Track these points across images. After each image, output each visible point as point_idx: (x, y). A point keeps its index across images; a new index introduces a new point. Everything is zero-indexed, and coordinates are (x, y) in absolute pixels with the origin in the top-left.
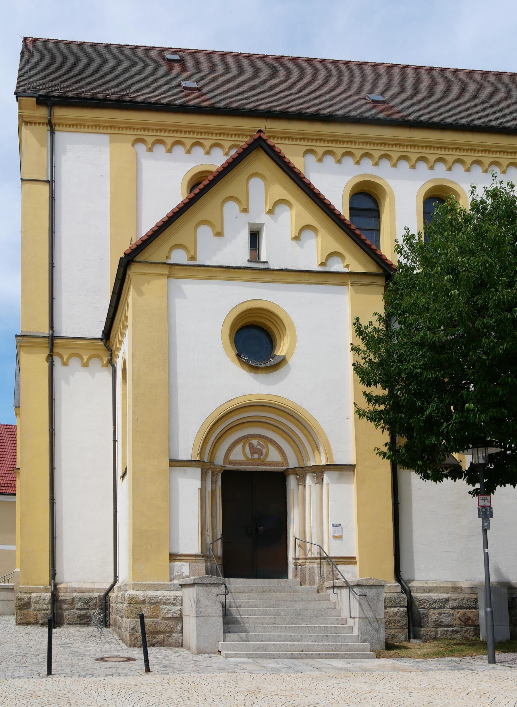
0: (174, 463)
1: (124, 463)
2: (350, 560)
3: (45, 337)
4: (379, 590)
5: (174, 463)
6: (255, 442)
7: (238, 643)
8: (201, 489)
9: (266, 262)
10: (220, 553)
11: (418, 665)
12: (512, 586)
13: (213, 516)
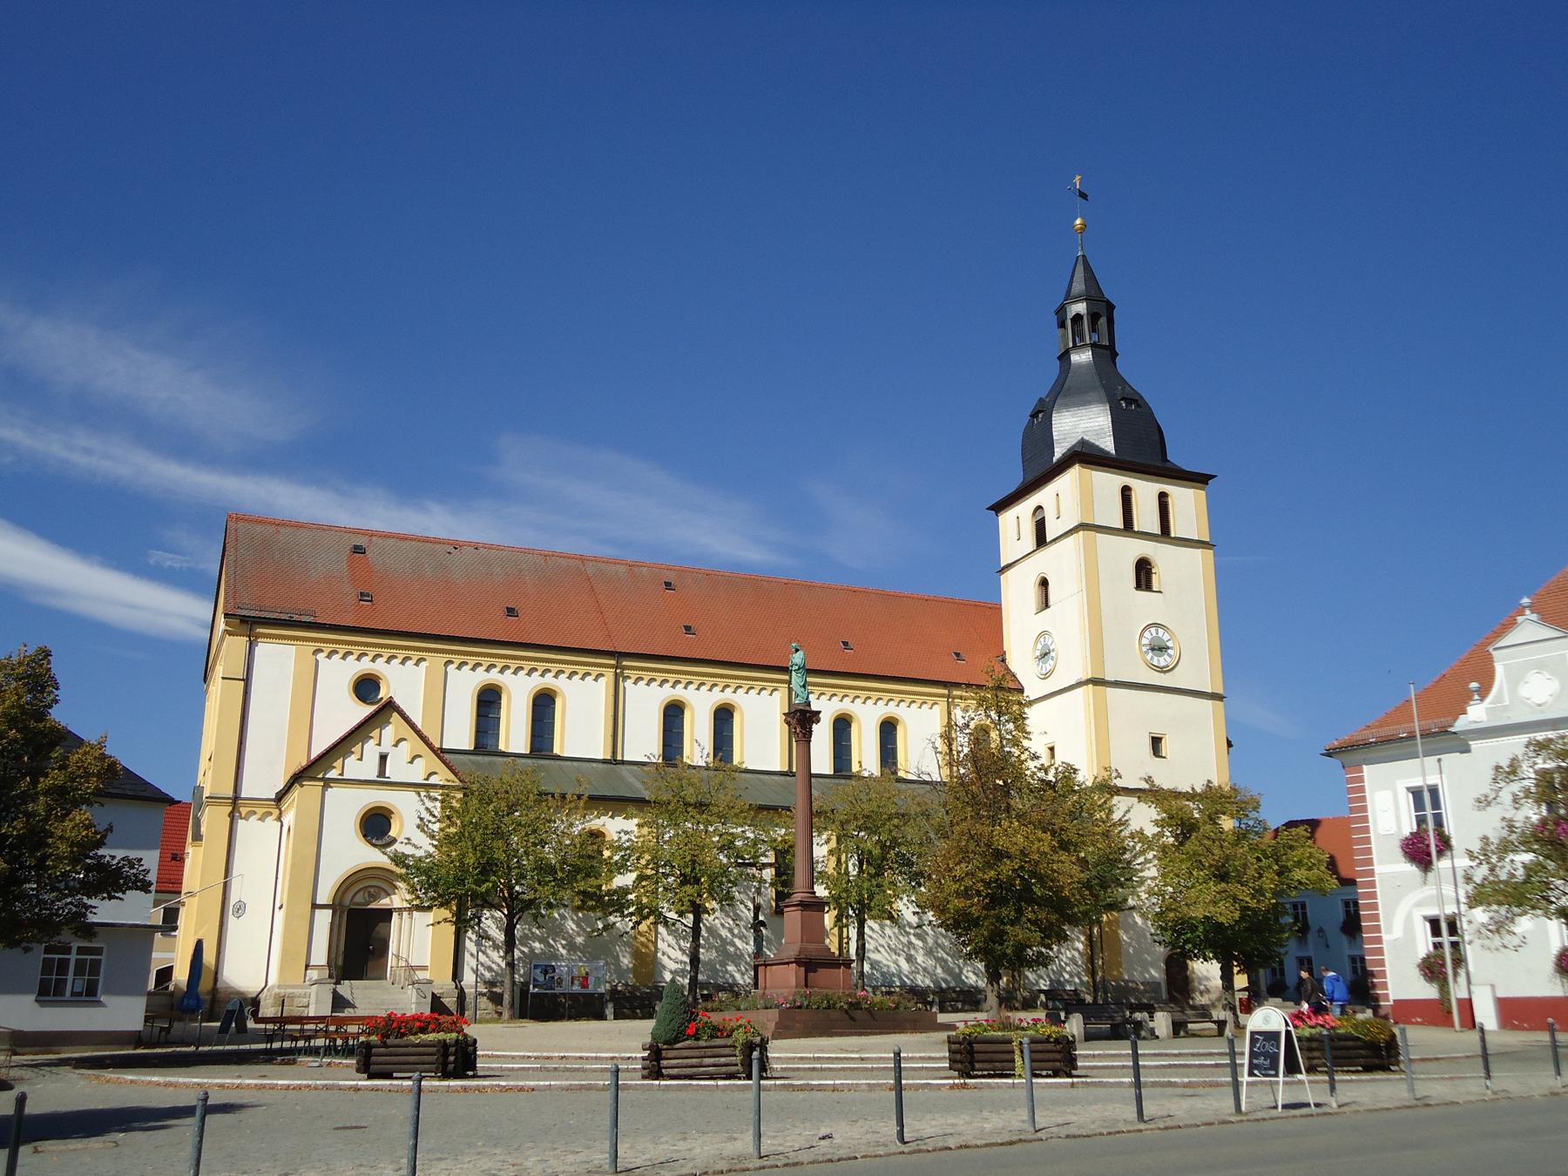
1: (282, 899)
2: (424, 968)
3: (229, 798)
6: (372, 890)
7: (508, 1053)
8: (331, 923)
9: (388, 778)
10: (774, 897)
12: (232, 988)
13: (338, 940)
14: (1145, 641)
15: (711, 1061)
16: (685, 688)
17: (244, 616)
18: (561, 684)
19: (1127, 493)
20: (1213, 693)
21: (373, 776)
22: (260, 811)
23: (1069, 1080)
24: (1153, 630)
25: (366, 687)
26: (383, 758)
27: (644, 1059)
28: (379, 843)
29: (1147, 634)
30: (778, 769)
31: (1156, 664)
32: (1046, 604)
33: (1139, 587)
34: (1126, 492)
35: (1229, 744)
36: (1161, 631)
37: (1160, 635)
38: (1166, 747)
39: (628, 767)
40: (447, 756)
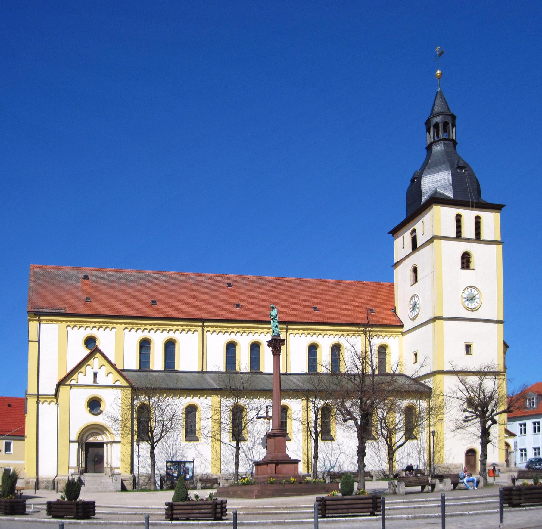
0: (70, 442)
2: (118, 468)
4: (120, 475)
5: (70, 442)
9: (98, 383)
11: (95, 478)
14: (465, 296)
15: (197, 511)
16: (149, 332)
17: (35, 312)
18: (176, 336)
19: (478, 220)
20: (498, 320)
21: (91, 382)
22: (49, 400)
23: (375, 517)
24: (469, 289)
25: (90, 341)
26: (95, 374)
27: (166, 510)
28: (96, 413)
29: (466, 292)
30: (196, 370)
31: (470, 307)
32: (416, 281)
33: (463, 267)
34: (458, 218)
35: (506, 346)
36: (473, 290)
37: (473, 292)
38: (473, 349)
39: (209, 374)
40: (124, 373)
